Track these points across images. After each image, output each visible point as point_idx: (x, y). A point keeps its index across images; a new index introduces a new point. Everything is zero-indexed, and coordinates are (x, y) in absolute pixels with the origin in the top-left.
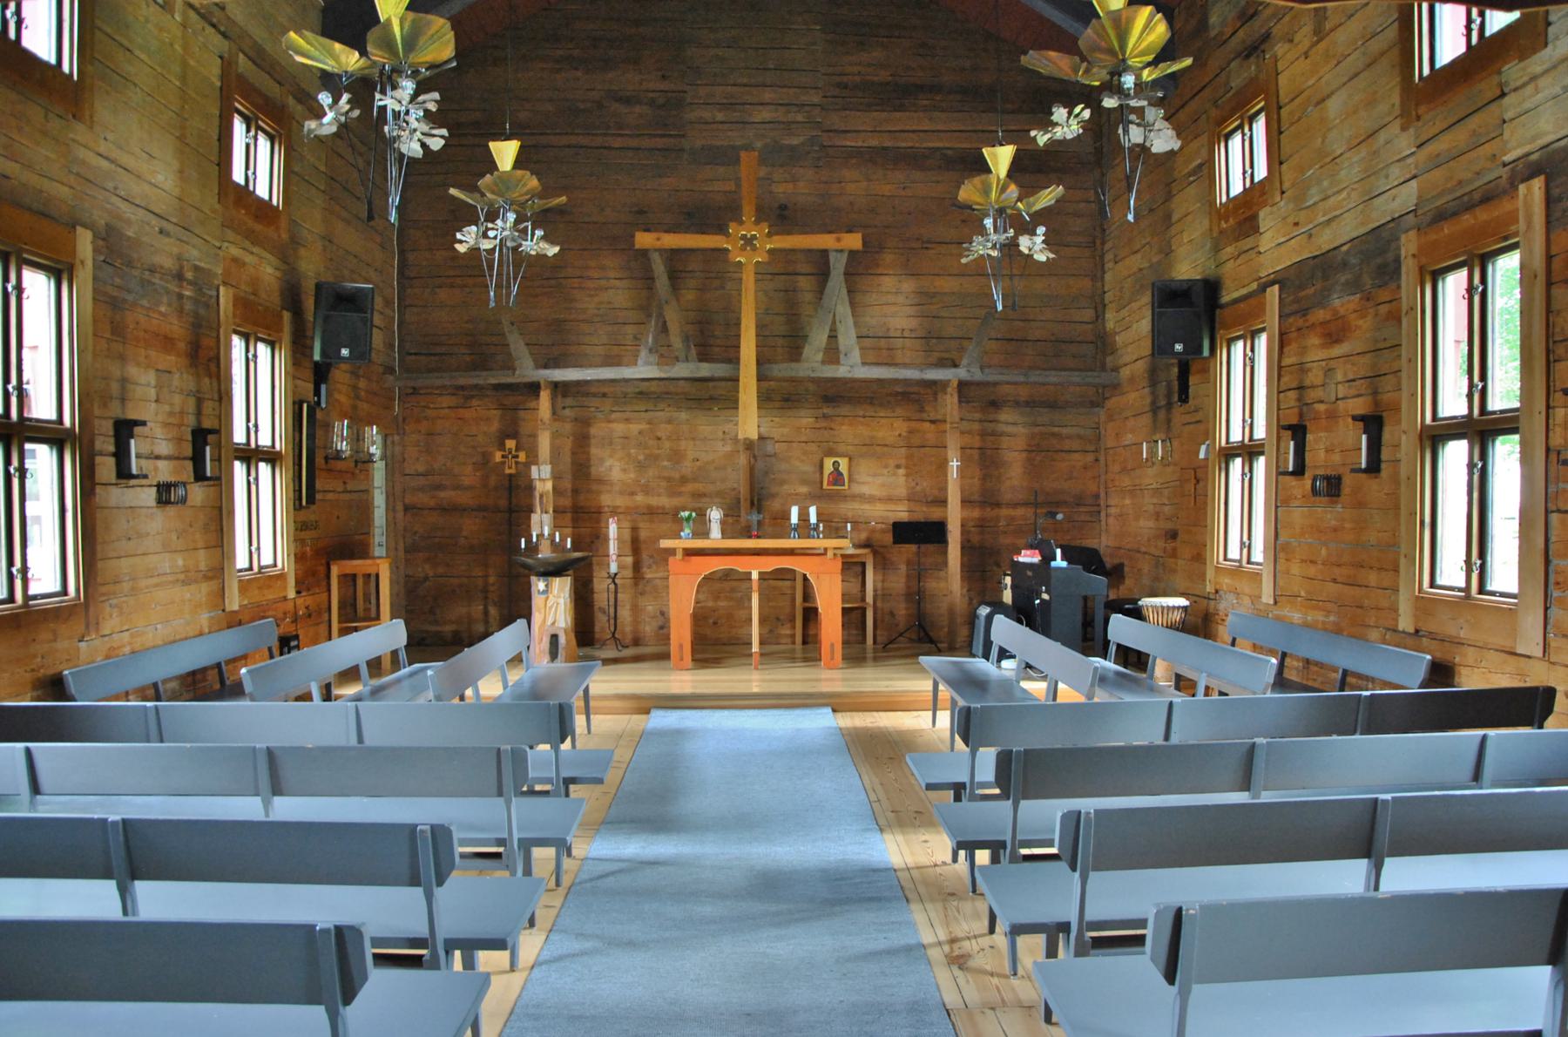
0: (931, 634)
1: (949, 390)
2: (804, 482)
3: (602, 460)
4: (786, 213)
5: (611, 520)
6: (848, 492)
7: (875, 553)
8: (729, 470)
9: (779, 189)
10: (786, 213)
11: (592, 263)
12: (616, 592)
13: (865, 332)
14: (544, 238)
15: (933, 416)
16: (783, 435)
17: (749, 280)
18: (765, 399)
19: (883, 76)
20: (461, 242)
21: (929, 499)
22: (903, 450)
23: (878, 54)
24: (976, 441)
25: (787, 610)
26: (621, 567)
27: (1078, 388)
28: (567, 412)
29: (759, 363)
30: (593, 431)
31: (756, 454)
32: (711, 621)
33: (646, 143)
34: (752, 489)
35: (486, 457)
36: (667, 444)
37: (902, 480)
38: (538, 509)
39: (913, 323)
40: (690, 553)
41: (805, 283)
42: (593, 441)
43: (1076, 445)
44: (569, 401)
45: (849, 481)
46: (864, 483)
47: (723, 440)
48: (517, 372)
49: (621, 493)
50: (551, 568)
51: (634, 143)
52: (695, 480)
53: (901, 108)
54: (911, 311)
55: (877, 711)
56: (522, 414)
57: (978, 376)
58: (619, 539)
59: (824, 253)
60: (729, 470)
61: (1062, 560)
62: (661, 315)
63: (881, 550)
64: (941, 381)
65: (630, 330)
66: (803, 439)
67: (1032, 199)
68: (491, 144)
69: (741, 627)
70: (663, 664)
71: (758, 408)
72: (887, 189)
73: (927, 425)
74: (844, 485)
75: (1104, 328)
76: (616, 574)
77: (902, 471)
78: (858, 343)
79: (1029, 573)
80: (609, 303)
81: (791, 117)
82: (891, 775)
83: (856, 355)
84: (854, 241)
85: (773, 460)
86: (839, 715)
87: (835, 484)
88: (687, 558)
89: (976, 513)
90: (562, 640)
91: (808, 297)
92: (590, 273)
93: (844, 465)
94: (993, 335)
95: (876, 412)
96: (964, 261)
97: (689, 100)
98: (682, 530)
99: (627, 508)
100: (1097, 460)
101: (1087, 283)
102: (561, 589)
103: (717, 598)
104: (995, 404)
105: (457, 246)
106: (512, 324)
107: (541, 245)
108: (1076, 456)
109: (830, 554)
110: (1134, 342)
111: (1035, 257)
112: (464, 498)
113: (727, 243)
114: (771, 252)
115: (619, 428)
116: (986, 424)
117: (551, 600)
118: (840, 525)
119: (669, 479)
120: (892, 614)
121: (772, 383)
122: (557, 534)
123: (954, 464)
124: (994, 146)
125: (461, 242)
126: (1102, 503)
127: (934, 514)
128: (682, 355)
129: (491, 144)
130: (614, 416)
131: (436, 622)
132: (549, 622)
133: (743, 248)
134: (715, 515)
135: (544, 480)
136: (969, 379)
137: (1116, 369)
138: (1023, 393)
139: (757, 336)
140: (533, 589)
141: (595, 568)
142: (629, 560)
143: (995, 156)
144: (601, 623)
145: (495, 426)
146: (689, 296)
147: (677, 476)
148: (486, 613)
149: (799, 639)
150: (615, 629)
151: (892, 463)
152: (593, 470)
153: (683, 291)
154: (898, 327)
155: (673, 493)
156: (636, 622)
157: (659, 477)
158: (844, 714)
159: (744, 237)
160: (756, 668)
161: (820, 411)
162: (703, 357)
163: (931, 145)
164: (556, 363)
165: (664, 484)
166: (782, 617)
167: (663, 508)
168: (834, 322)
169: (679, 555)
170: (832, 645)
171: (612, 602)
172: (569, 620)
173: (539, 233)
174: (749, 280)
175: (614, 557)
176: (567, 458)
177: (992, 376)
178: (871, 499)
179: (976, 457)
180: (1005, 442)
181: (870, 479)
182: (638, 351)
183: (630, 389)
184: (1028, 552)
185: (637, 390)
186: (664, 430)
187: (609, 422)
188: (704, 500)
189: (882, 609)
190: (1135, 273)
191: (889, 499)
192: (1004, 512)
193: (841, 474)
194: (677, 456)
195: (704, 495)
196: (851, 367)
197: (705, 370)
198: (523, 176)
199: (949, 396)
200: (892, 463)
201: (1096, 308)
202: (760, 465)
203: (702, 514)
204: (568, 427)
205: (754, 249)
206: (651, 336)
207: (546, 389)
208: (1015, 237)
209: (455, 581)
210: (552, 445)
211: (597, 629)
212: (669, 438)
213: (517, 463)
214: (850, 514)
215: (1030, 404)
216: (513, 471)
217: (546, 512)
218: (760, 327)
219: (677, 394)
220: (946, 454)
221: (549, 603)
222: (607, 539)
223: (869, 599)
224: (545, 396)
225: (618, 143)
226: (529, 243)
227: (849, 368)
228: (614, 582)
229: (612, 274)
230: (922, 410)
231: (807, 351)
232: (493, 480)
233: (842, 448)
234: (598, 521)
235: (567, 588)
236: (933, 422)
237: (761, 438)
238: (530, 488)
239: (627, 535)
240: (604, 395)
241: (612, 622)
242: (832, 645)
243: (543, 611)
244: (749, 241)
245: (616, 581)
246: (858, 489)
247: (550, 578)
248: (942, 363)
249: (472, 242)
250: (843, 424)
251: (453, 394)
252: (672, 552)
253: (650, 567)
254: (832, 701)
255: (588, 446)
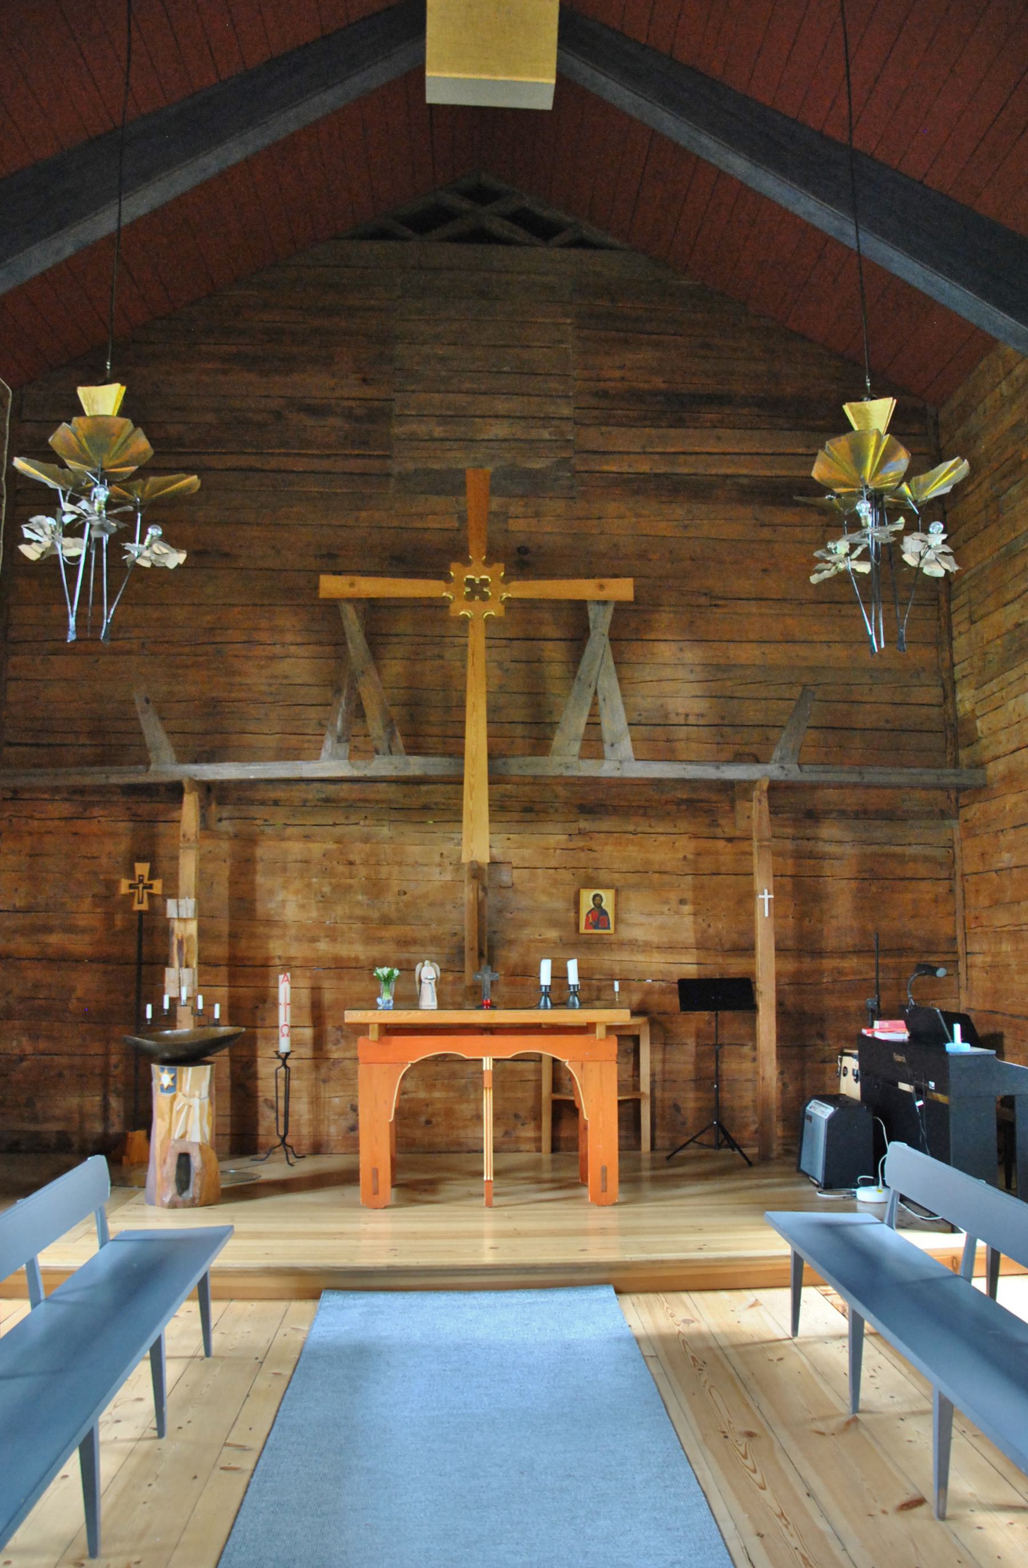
0: (733, 1135)
1: (756, 794)
2: (554, 923)
3: (271, 892)
4: (525, 558)
5: (281, 977)
6: (613, 938)
7: (653, 1023)
8: (449, 907)
9: (516, 525)
10: (525, 558)
11: (264, 623)
12: (287, 1079)
13: (636, 718)
14: (165, 538)
15: (729, 832)
16: (523, 859)
17: (477, 641)
18: (499, 808)
19: (659, 383)
20: (29, 542)
21: (727, 946)
22: (690, 878)
23: (647, 356)
24: (789, 866)
25: (530, 1103)
26: (295, 1042)
27: (923, 793)
28: (226, 826)
29: (491, 757)
30: (260, 852)
31: (486, 884)
32: (423, 1119)
33: (341, 465)
34: (480, 931)
35: (112, 886)
36: (362, 872)
37: (689, 920)
38: (176, 963)
39: (700, 706)
40: (390, 1030)
41: (554, 652)
42: (260, 867)
43: (922, 870)
44: (226, 811)
45: (616, 923)
46: (635, 925)
47: (440, 865)
48: (152, 767)
49: (298, 939)
50: (181, 1053)
51: (325, 465)
52: (403, 921)
53: (679, 423)
54: (697, 689)
55: (687, 1291)
56: (162, 827)
57: (793, 773)
58: (294, 1003)
59: (580, 606)
60: (449, 907)
61: (963, 1041)
62: (353, 689)
63: (662, 1018)
64: (740, 782)
65: (313, 713)
66: (553, 863)
67: (922, 478)
68: (82, 392)
69: (465, 1127)
70: (349, 1193)
71: (490, 821)
72: (663, 528)
73: (721, 844)
74: (609, 928)
75: (955, 710)
76: (288, 1054)
77: (687, 908)
78: (630, 731)
79: (899, 1058)
80: (286, 677)
81: (534, 434)
82: (767, 1495)
83: (626, 747)
84: (623, 589)
85: (510, 894)
86: (628, 1300)
87: (595, 927)
88: (386, 1038)
89: (790, 966)
90: (196, 1162)
91: (556, 670)
92: (263, 636)
93: (608, 899)
94: (812, 722)
95: (650, 826)
96: (814, 579)
97: (397, 411)
98: (380, 995)
99: (306, 959)
100: (951, 891)
101: (928, 654)
102: (196, 1084)
103: (431, 1087)
104: (813, 816)
105: (24, 548)
106: (147, 701)
107: (155, 548)
108: (923, 885)
109: (600, 1031)
110: (1010, 725)
111: (927, 571)
112: (79, 945)
113: (447, 590)
114: (510, 604)
115: (296, 848)
116: (799, 842)
117: (180, 1102)
118: (605, 983)
119: (364, 920)
120: (676, 1108)
121: (509, 787)
122: (200, 998)
123: (765, 897)
124: (861, 400)
125: (29, 542)
126: (960, 949)
127: (735, 967)
128: (382, 745)
129: (82, 392)
130: (289, 831)
131: (35, 1119)
132: (176, 1135)
133: (470, 597)
134: (428, 972)
135: (185, 920)
136: (782, 778)
137: (981, 765)
138: (852, 800)
139: (489, 722)
140: (155, 1083)
141: (260, 1044)
142: (308, 1033)
143: (864, 415)
144: (267, 1122)
145: (123, 846)
146: (395, 668)
147: (376, 915)
148: (106, 1107)
149: (546, 1144)
150: (286, 1134)
151: (674, 897)
152: (260, 908)
153: (385, 661)
154: (681, 710)
155: (369, 940)
156: (317, 1121)
157: (350, 917)
158: (634, 1298)
159: (470, 583)
160: (489, 1205)
161: (574, 825)
162: (414, 749)
163: (722, 471)
164: (211, 757)
165: (358, 926)
166: (522, 1114)
167: (357, 959)
168: (595, 704)
169: (374, 1035)
170: (604, 1170)
171: (281, 1094)
172: (207, 1130)
173: (154, 531)
174: (477, 641)
175: (285, 1030)
176: (222, 890)
177: (809, 776)
178: (646, 947)
179: (789, 888)
180: (828, 868)
181: (643, 919)
182: (322, 742)
183: (312, 793)
184: (886, 1024)
185: (323, 796)
186: (358, 852)
187: (283, 840)
188: (413, 949)
189: (663, 1101)
190: (1009, 632)
191: (671, 948)
192: (829, 963)
193: (605, 913)
194: (376, 888)
195: (414, 942)
196: (621, 762)
197: (415, 766)
198: (123, 428)
199: (755, 804)
200: (674, 897)
201: (943, 686)
202: (492, 900)
203: (408, 968)
204: (225, 847)
205: (484, 597)
206: (340, 717)
207: (190, 793)
208: (899, 535)
209: (64, 1060)
210: (201, 873)
211: (262, 1131)
212: (366, 863)
213: (151, 896)
214: (617, 968)
215: (862, 814)
216: (144, 907)
217: (187, 966)
218: (493, 711)
219: (377, 802)
220: (752, 884)
221: (177, 1107)
222: (276, 1004)
223: (645, 1087)
224: (190, 804)
225: (301, 465)
226: (137, 545)
227: (618, 765)
228: (285, 1065)
229: (289, 638)
230: (714, 823)
231: (558, 740)
232: (119, 920)
233: (604, 876)
234: (265, 977)
235: (206, 1083)
236: (730, 840)
237: (493, 863)
238: (167, 931)
239: (305, 996)
240: (276, 803)
241: (282, 1120)
242: (604, 1170)
243: (167, 1117)
244: (477, 590)
245: (289, 1063)
246: (628, 933)
247: (179, 1068)
248: (739, 758)
249: (47, 542)
250: (606, 844)
251: (67, 800)
252: (362, 1029)
253: (337, 1042)
254: (614, 1275)
255: (255, 872)
